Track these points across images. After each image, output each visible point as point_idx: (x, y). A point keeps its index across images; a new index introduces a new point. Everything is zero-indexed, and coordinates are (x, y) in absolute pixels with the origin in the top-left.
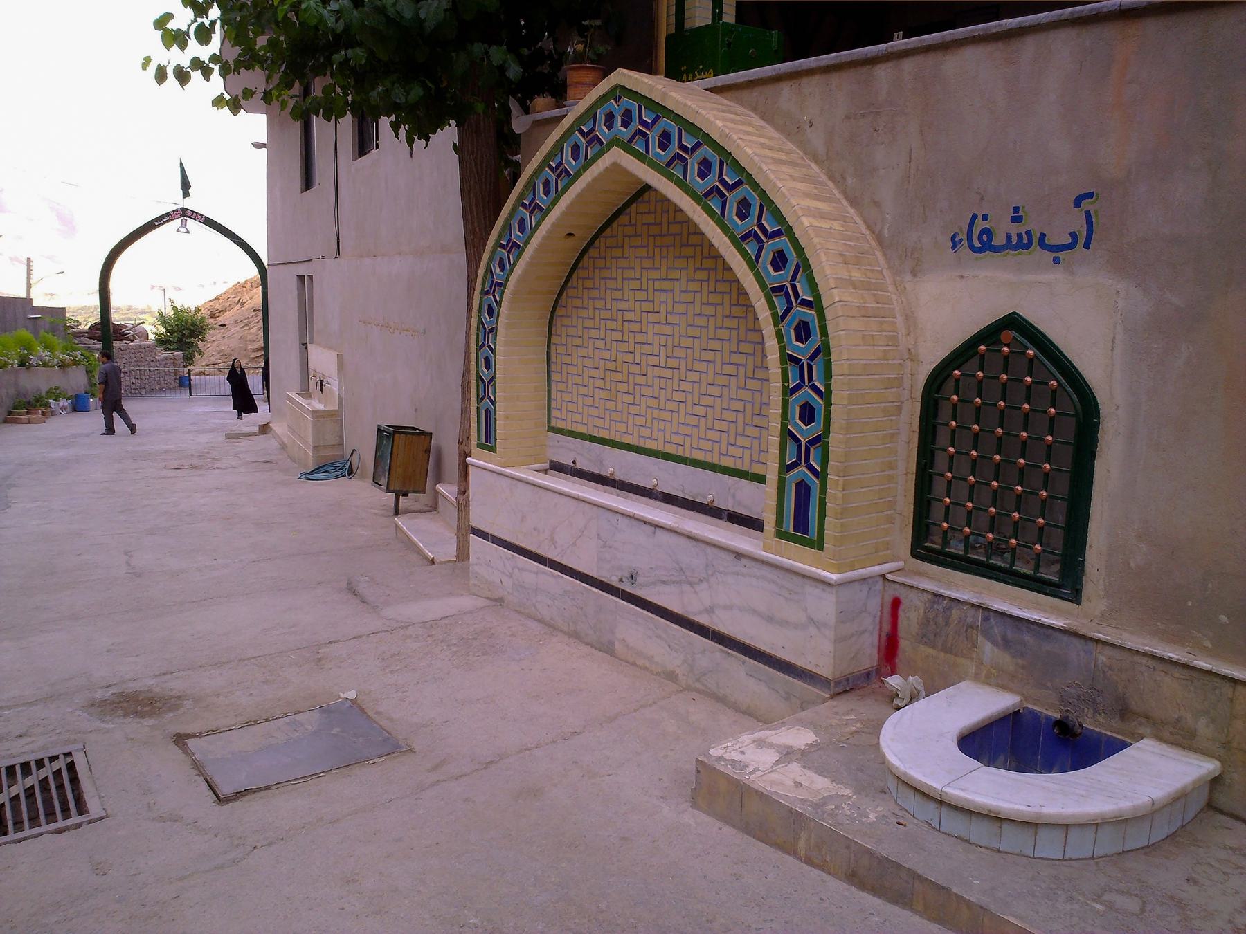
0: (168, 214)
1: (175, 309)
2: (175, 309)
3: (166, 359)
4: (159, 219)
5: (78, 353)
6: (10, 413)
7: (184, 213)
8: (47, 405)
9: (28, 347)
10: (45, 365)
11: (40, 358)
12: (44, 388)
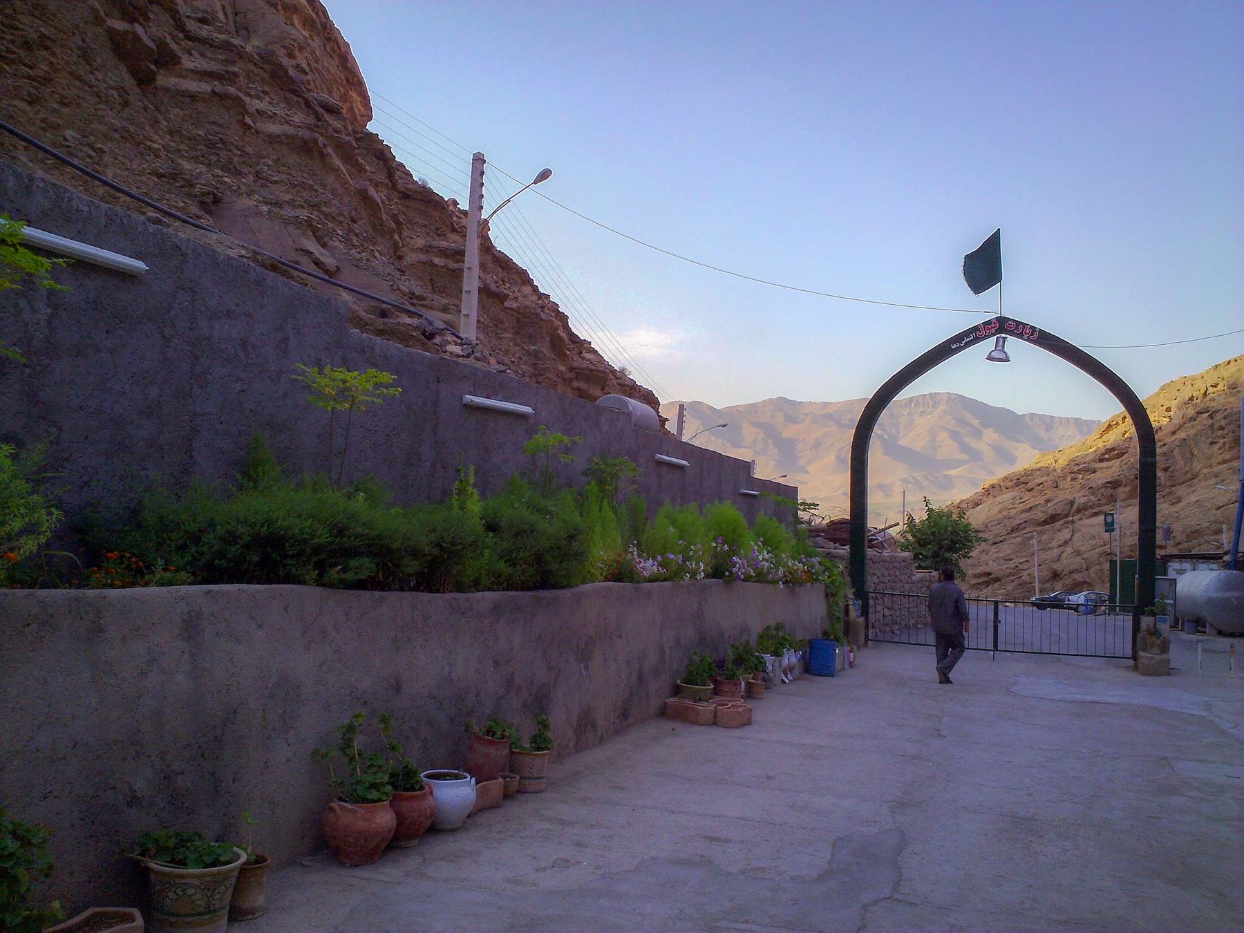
0: (975, 329)
1: (930, 511)
2: (930, 511)
3: (922, 580)
4: (959, 338)
5: (815, 560)
6: (677, 691)
7: (1003, 326)
8: (759, 667)
9: (732, 539)
10: (761, 577)
11: (755, 564)
12: (756, 626)
